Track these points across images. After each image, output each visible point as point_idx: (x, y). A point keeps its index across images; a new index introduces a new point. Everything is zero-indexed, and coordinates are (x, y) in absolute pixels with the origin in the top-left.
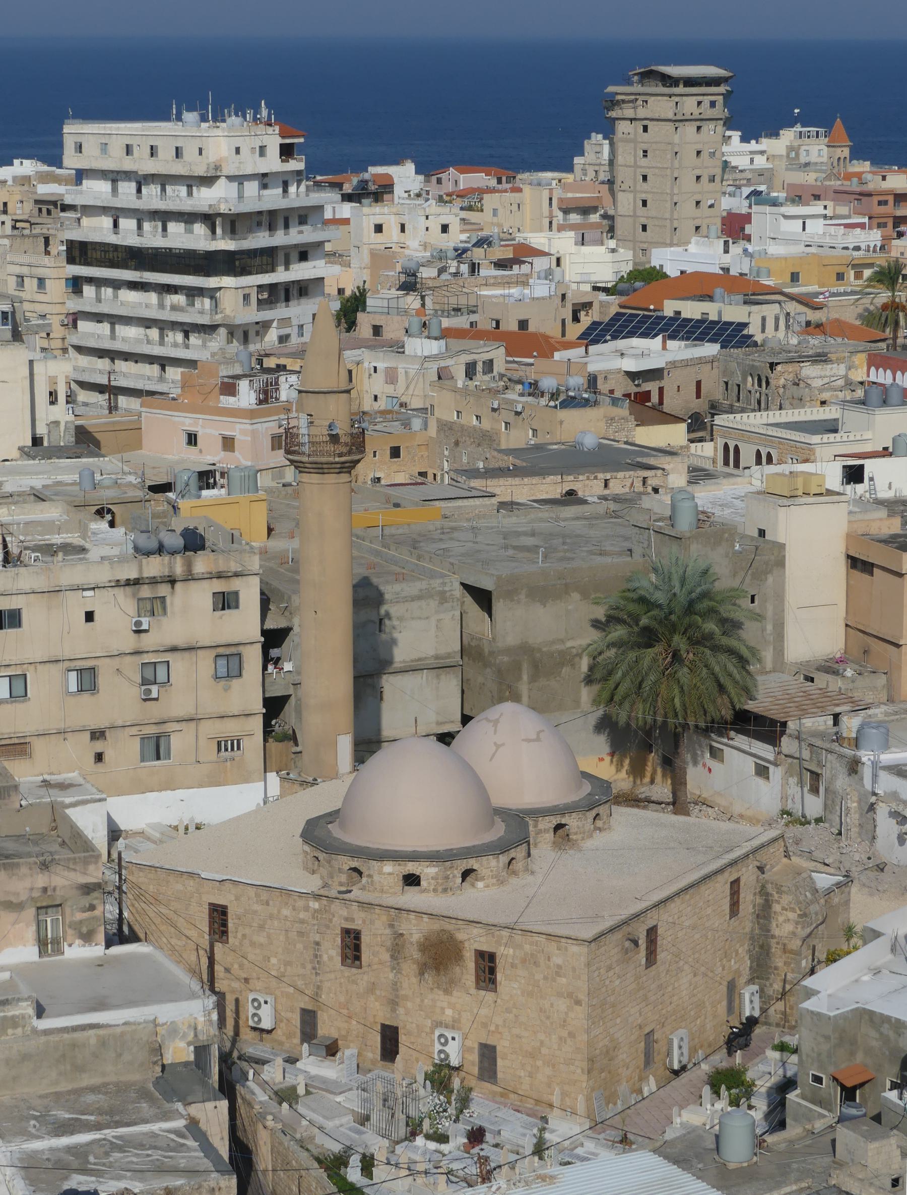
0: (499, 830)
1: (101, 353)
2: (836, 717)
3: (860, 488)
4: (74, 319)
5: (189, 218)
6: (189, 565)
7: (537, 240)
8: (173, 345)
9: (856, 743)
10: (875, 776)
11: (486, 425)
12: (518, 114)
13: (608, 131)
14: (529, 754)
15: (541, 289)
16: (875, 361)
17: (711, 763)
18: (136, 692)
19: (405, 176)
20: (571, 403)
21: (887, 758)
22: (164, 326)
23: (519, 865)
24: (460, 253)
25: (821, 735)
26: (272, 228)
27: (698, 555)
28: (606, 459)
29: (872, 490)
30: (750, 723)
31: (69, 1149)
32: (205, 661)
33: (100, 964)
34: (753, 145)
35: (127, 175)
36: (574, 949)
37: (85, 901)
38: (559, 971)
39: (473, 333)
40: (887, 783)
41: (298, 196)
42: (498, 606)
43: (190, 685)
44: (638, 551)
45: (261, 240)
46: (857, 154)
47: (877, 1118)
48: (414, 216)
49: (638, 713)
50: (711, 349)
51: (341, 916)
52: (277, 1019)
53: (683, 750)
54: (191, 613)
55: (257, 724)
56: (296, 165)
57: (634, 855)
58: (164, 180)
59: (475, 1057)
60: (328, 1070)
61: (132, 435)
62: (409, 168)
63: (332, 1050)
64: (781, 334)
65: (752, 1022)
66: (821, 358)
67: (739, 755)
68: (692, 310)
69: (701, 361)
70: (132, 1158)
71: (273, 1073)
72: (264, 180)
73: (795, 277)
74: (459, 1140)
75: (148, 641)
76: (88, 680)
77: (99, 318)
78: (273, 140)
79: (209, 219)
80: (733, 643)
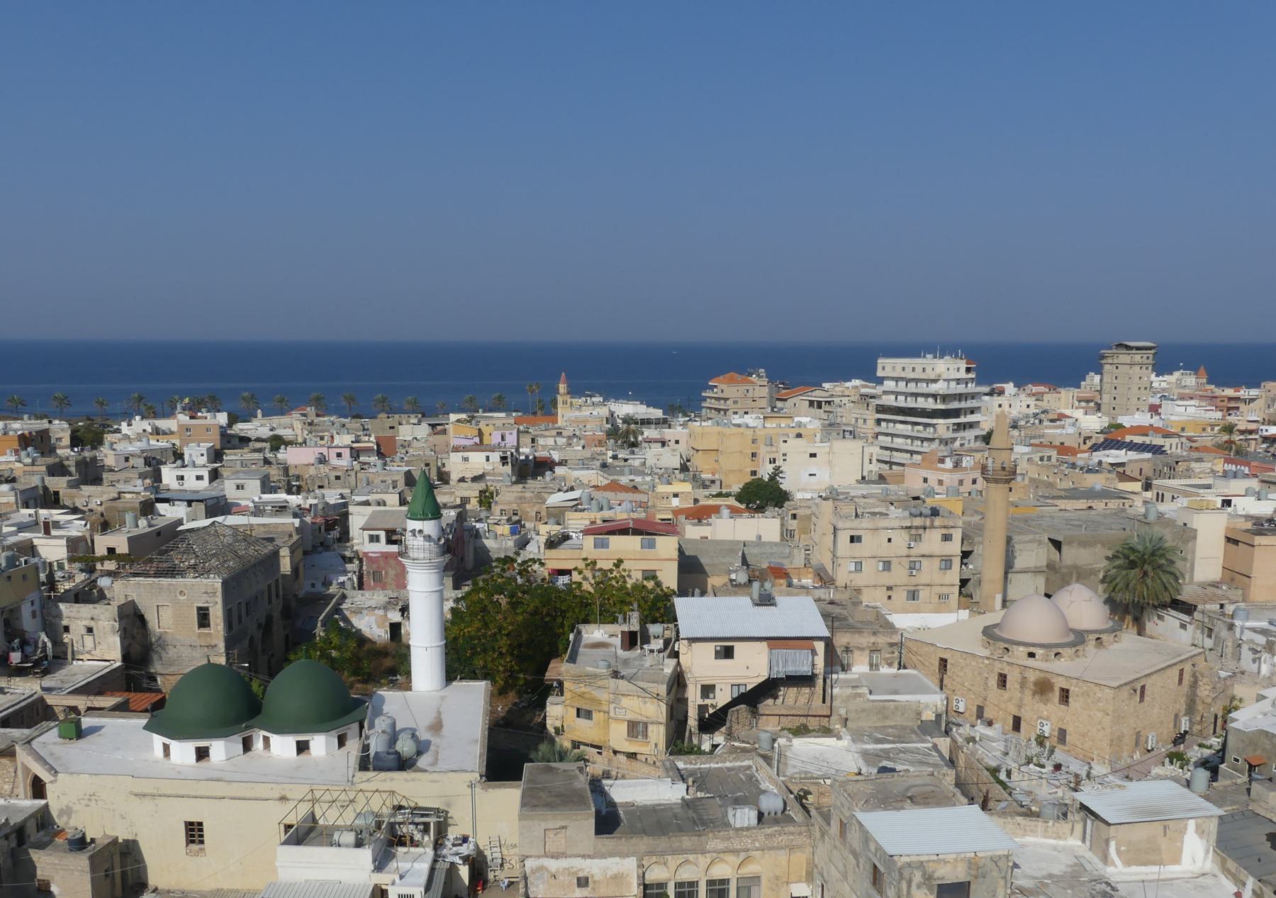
0: (1071, 638)
1: (886, 448)
2: (1222, 606)
3: (1229, 509)
4: (877, 435)
5: (926, 396)
6: (932, 522)
7: (1067, 412)
9: (1232, 617)
10: (1242, 632)
11: (1051, 479)
12: (1061, 366)
13: (1099, 371)
14: (1084, 607)
15: (1070, 430)
16: (1227, 461)
17: (1159, 622)
18: (907, 572)
19: (1009, 388)
20: (1089, 471)
21: (1248, 624)
22: (913, 438)
23: (1080, 653)
24: (1035, 415)
25: (1214, 612)
26: (960, 400)
27: (1157, 531)
28: (1105, 494)
29: (1235, 510)
30: (1177, 605)
31: (881, 750)
32: (937, 561)
33: (895, 676)
34: (1161, 378)
35: (902, 379)
36: (1108, 691)
37: (890, 650)
38: (1099, 700)
39: (1041, 445)
40: (1248, 635)
41: (972, 388)
42: (1064, 548)
43: (929, 571)
44: (1128, 529)
45: (955, 405)
46: (1209, 382)
47: (1270, 780)
48: (1014, 402)
49: (1127, 597)
50: (1148, 455)
51: (999, 667)
52: (966, 709)
53: (1145, 614)
54: (932, 542)
55: (957, 588)
56: (972, 375)
57: (1129, 653)
58: (917, 381)
59: (1056, 733)
60: (988, 732)
61: (900, 478)
62: (1011, 385)
63: (990, 724)
64: (1179, 450)
65: (1186, 732)
66: (1200, 460)
67: (1172, 619)
68: (1138, 440)
69: (1142, 460)
70: (909, 756)
71: (966, 730)
72: (958, 381)
73: (1183, 429)
74: (1049, 768)
75: (912, 552)
76: (887, 565)
77: (887, 435)
78: (963, 365)
79: (934, 396)
80: (1172, 570)
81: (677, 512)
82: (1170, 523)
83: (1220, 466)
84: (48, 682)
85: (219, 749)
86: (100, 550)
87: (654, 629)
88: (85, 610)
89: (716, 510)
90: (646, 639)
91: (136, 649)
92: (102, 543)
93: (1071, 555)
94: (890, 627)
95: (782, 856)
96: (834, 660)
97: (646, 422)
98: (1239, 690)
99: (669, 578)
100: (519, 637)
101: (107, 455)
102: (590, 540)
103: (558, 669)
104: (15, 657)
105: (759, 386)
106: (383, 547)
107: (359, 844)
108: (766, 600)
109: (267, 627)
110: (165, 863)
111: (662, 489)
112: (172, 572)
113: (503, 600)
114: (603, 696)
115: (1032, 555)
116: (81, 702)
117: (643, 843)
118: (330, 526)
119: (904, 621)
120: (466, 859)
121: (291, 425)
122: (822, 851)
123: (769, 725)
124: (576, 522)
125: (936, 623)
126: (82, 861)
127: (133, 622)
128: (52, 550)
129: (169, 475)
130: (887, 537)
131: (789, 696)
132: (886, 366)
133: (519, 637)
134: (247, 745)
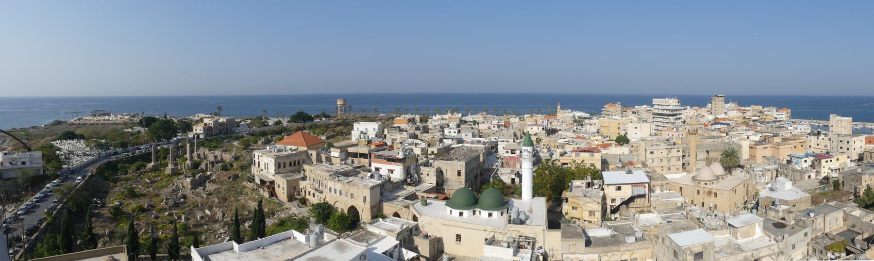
8: (665, 125)
12: (700, 101)
13: (711, 103)
19: (688, 107)
28: (717, 137)
30: (740, 166)
41: (680, 108)
43: (674, 161)
48: (689, 112)
51: (697, 188)
54: (674, 152)
61: (661, 134)
67: (739, 170)
71: (689, 208)
76: (661, 160)
81: (597, 145)
82: (735, 144)
83: (744, 128)
84: (417, 188)
85: (466, 213)
86: (430, 152)
87: (595, 181)
88: (427, 169)
89: (610, 145)
90: (593, 185)
91: (440, 181)
92: (430, 150)
93: (712, 155)
94: (665, 178)
95: (644, 251)
96: (651, 190)
97: (585, 118)
98: (758, 187)
99: (598, 166)
100: (554, 184)
101: (430, 125)
102: (574, 154)
103: (565, 194)
104: (409, 180)
105: (618, 107)
106: (510, 155)
107: (509, 247)
108: (630, 172)
109: (476, 177)
110: (450, 247)
111: (592, 138)
112: (451, 159)
113: (547, 172)
114: (581, 203)
115: (702, 155)
116: (426, 195)
117: (601, 249)
118: (492, 148)
119: (668, 176)
120: (542, 254)
121: (479, 117)
122: (656, 248)
123: (632, 211)
124: (569, 148)
125: (676, 176)
126: (427, 242)
127: (440, 173)
128: (417, 151)
129: (446, 131)
130: (661, 152)
131: (638, 201)
132: (655, 101)
133: (554, 184)
134: (474, 213)
